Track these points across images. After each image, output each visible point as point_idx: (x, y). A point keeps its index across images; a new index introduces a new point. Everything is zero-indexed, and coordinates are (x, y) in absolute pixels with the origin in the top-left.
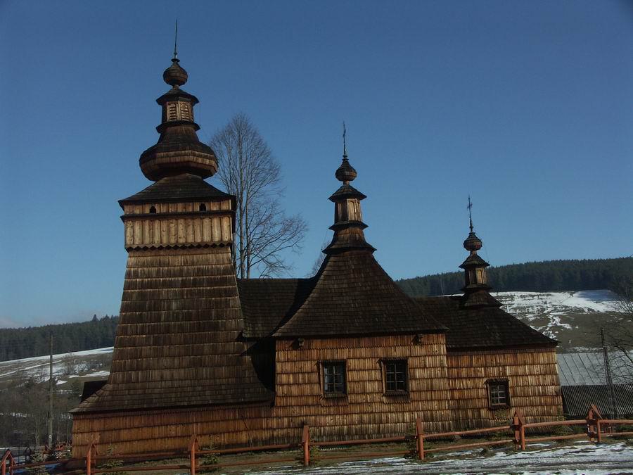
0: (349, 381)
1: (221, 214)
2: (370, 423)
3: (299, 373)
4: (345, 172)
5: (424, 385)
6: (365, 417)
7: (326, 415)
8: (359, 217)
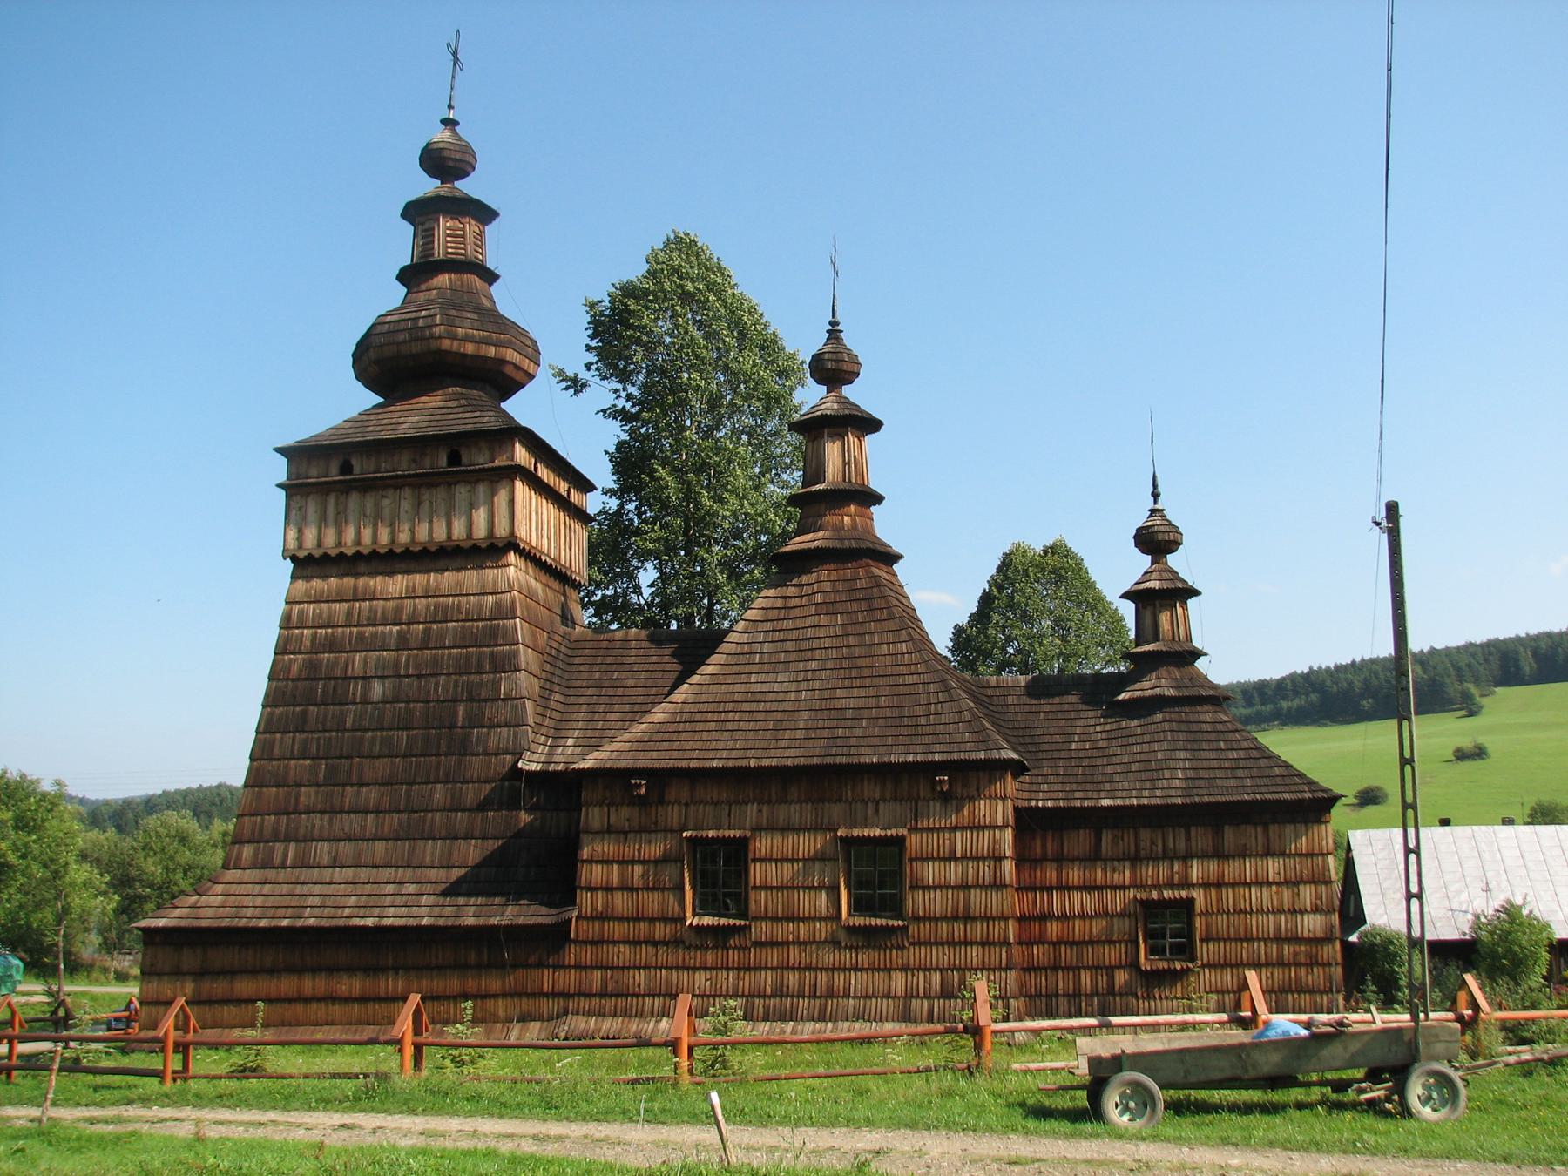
0: (755, 887)
2: (801, 995)
4: (444, 162)
5: (940, 902)
6: (791, 979)
7: (695, 969)
8: (860, 471)
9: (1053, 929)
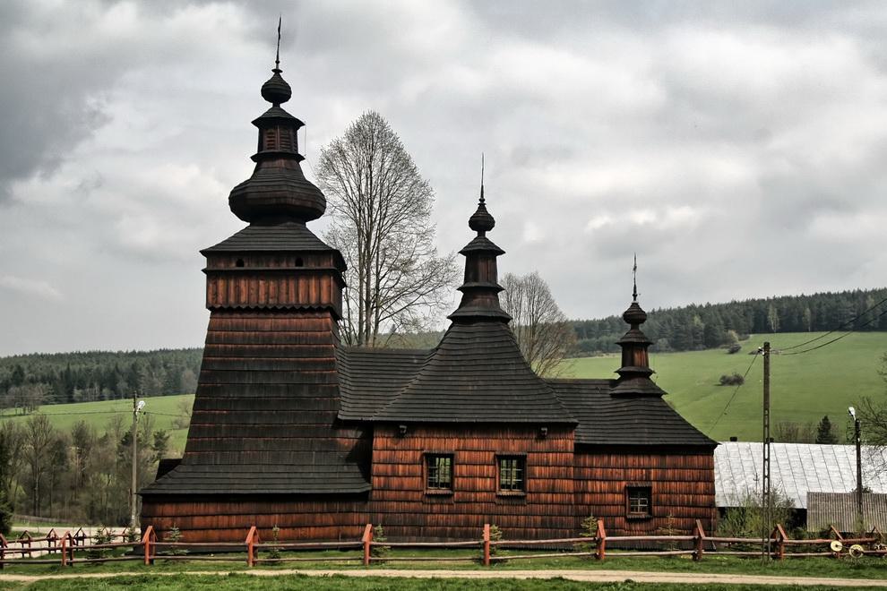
1: (319, 274)
3: (398, 464)
9: (587, 498)
